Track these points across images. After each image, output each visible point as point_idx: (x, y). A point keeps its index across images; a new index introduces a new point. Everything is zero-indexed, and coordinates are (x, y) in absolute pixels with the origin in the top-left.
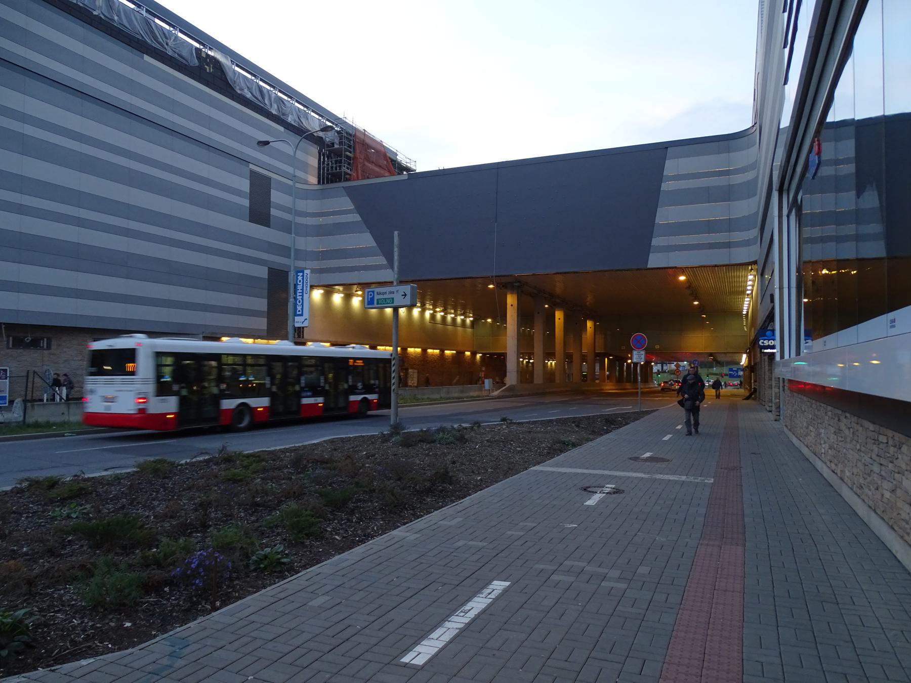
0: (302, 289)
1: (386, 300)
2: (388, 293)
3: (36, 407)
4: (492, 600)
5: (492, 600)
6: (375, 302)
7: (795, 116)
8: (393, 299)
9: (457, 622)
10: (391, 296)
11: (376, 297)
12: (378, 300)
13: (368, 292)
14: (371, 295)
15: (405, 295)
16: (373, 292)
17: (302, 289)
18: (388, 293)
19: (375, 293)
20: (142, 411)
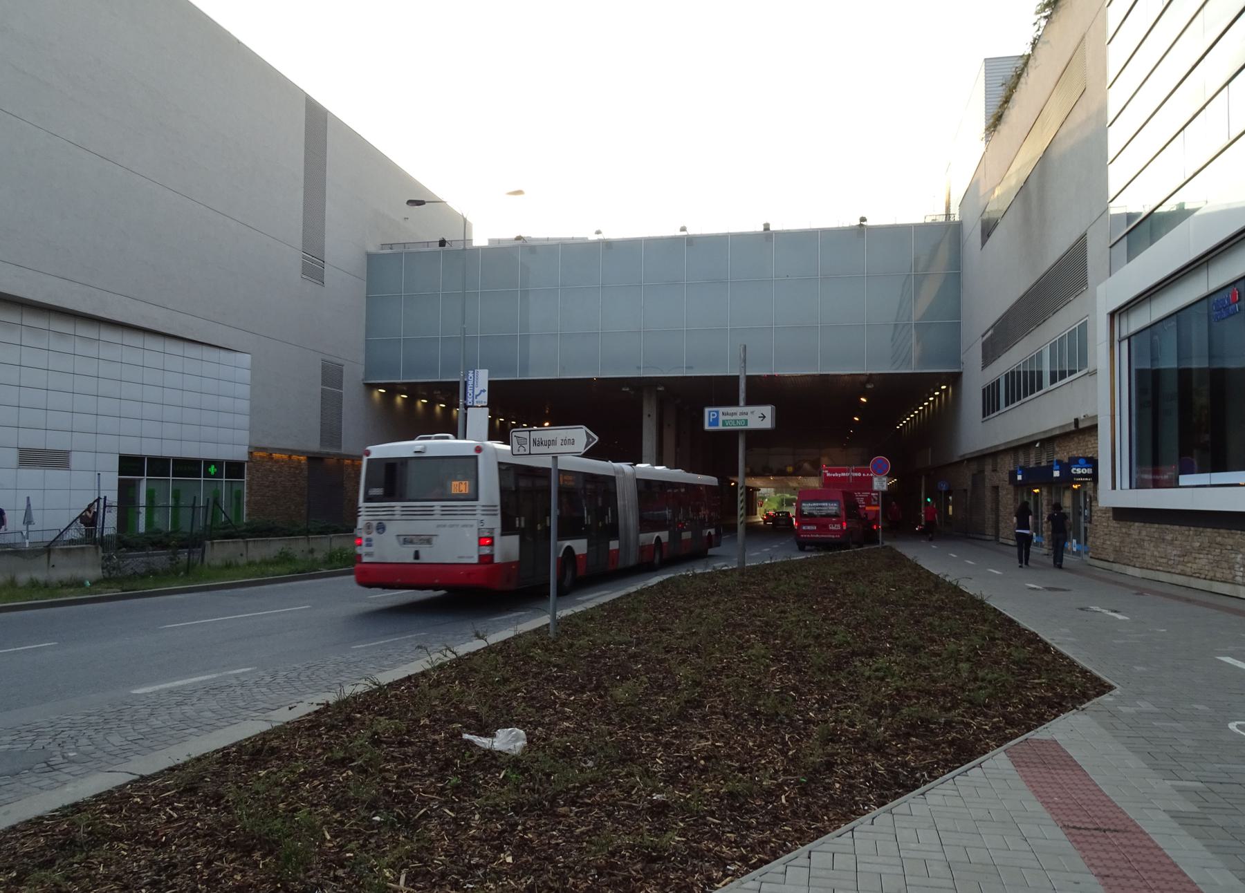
0: (473, 384)
1: (736, 423)
2: (559, 442)
3: (215, 545)
4: (1111, 196)
5: (1111, 196)
6: (721, 423)
7: (502, 245)
8: (746, 421)
9: (923, 486)
10: (744, 417)
11: (721, 418)
12: (724, 421)
13: (710, 412)
14: (714, 415)
15: (764, 417)
16: (717, 412)
17: (473, 384)
18: (559, 442)
19: (721, 414)
20: (486, 559)
